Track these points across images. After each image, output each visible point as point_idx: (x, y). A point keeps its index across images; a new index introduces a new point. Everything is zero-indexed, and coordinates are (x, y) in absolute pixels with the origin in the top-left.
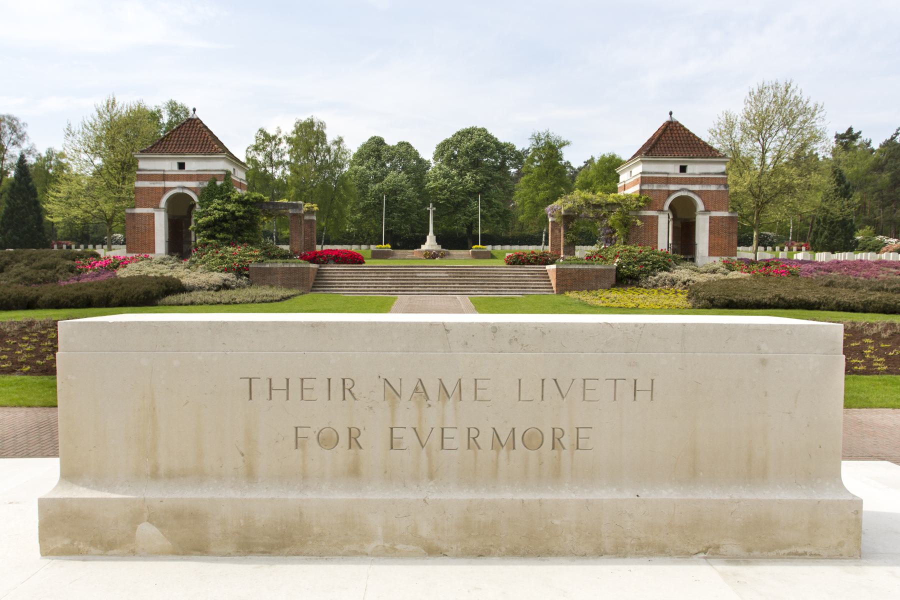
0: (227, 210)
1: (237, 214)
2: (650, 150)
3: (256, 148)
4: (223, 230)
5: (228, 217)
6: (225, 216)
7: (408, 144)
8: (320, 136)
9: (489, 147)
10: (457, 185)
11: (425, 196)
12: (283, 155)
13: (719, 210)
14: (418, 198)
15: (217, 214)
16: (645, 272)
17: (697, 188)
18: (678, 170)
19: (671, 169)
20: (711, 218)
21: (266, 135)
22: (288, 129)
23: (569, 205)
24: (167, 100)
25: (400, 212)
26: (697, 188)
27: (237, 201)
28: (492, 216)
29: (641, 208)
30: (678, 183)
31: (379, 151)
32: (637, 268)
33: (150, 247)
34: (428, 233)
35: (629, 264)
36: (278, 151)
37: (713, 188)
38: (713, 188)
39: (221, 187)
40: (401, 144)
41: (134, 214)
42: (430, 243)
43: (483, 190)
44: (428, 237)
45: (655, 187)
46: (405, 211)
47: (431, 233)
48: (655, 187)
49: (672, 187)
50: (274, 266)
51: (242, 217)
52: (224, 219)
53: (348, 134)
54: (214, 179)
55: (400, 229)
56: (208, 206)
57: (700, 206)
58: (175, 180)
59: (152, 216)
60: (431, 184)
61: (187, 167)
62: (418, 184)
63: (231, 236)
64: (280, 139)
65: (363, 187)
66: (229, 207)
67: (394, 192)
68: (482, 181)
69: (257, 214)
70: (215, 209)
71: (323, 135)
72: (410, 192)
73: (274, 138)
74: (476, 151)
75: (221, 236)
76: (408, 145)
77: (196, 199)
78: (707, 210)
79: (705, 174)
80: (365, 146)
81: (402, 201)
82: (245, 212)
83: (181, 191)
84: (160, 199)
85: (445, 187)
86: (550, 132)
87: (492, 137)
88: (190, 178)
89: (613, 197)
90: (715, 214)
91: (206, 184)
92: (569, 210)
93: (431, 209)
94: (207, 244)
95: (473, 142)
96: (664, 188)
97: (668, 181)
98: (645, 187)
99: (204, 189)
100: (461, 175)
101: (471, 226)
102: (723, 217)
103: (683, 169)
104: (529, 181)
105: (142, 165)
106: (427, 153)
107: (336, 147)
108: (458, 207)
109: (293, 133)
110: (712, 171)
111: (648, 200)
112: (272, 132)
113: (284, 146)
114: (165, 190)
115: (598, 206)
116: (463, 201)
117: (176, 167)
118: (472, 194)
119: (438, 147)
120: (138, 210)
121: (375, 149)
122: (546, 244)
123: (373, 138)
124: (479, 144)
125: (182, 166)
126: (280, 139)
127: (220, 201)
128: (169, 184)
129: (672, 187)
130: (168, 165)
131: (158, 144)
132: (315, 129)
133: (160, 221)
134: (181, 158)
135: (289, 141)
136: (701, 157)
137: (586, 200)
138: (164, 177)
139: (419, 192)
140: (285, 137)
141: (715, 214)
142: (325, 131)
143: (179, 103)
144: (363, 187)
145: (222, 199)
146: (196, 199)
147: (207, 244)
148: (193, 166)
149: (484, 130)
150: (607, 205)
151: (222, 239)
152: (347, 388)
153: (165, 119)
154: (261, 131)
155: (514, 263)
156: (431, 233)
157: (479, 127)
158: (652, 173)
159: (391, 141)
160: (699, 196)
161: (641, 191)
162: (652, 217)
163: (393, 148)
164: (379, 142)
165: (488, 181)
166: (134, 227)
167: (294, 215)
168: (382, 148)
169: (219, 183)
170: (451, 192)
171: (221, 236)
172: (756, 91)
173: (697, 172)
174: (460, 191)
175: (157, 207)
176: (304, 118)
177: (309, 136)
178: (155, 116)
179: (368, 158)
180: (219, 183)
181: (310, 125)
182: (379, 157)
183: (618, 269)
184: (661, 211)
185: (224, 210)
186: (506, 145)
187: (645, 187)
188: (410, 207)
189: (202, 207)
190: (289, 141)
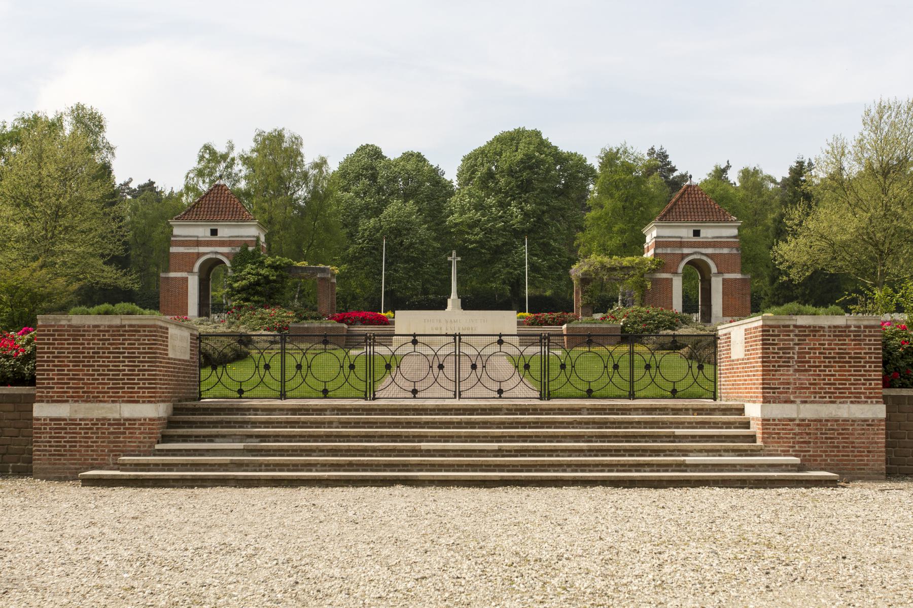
0: (261, 275)
1: (271, 278)
2: (665, 215)
3: (200, 173)
4: (257, 293)
5: (262, 281)
6: (259, 280)
7: (419, 155)
8: (293, 155)
9: (543, 162)
10: (495, 220)
11: (442, 232)
12: (238, 181)
13: (732, 272)
14: (435, 239)
15: (252, 279)
16: (647, 330)
17: (710, 251)
18: (691, 234)
19: (685, 233)
20: (724, 280)
21: (213, 153)
22: (245, 145)
23: (585, 268)
24: (72, 104)
25: (406, 262)
26: (710, 251)
27: (269, 266)
28: (550, 268)
29: (655, 271)
30: (691, 247)
31: (373, 168)
32: (641, 327)
33: (182, 309)
34: (449, 295)
35: (635, 323)
36: (229, 176)
37: (725, 251)
38: (725, 251)
39: (253, 252)
40: (408, 156)
41: (168, 278)
42: (453, 300)
43: (534, 230)
44: (449, 301)
45: (669, 251)
46: (413, 260)
47: (454, 295)
48: (669, 251)
49: (686, 251)
50: (312, 325)
51: (274, 281)
52: (257, 283)
53: (327, 146)
54: (246, 245)
55: (407, 288)
56: (241, 271)
57: (714, 269)
58: (208, 246)
59: (186, 279)
60: (455, 218)
61: (220, 233)
62: (434, 217)
63: (263, 299)
64: (233, 160)
65: (351, 223)
66: (262, 272)
67: (398, 231)
68: (534, 212)
69: (287, 278)
70: (249, 273)
71: (299, 154)
72: (422, 230)
73: (224, 157)
74: (525, 168)
75: (256, 298)
76: (420, 158)
77: (228, 264)
78: (720, 273)
79: (717, 237)
80: (350, 160)
81: (411, 244)
82: (277, 276)
83: (214, 256)
84: (193, 264)
85: (476, 223)
86: (628, 146)
87: (547, 145)
88: (222, 243)
89: (629, 261)
90: (728, 276)
91: (238, 250)
92: (585, 274)
93: (454, 259)
94: (242, 306)
95: (519, 156)
96: (678, 251)
97: (681, 244)
98: (659, 251)
99: (236, 255)
100: (502, 205)
101: (517, 285)
102: (736, 279)
103: (697, 233)
104: (599, 218)
105: (176, 231)
106: (451, 175)
107: (316, 171)
108: (497, 252)
109: (253, 151)
110: (724, 235)
111: (662, 264)
112: (221, 149)
113: (240, 169)
114: (199, 255)
115: (613, 269)
116: (504, 244)
117: (208, 233)
118: (518, 234)
119: (467, 159)
120: (172, 275)
121: (368, 164)
122: (210, 269)
123: (363, 148)
124: (529, 157)
125: (214, 232)
126: (233, 160)
127: (254, 267)
128: (202, 249)
129: (686, 251)
130: (201, 232)
131: (189, 211)
132: (285, 145)
133: (193, 283)
134: (213, 225)
135: (246, 161)
136: (713, 221)
137: (601, 263)
138: (198, 243)
139: (435, 230)
140: (242, 157)
141: (728, 276)
142: (302, 150)
143: (87, 106)
144: (351, 223)
145: (254, 263)
146: (228, 264)
147: (242, 306)
148: (226, 232)
149: (538, 134)
150: (622, 268)
151: (257, 302)
152: (440, 321)
153: (68, 128)
154: (207, 148)
155: (533, 324)
156: (454, 295)
157: (529, 128)
158: (665, 237)
159: (392, 152)
160: (712, 259)
161: (655, 255)
162: (667, 279)
163: (397, 163)
164: (375, 153)
165: (543, 212)
166: (168, 291)
167: (322, 279)
168: (380, 164)
169: (250, 249)
170: (489, 231)
171: (256, 298)
172: (874, 112)
173: (709, 236)
174: (499, 229)
175: (191, 271)
176: (269, 129)
177: (277, 153)
178: (55, 126)
179: (358, 177)
180: (250, 249)
181: (278, 137)
182: (374, 178)
183: (623, 328)
184: (675, 273)
185: (258, 274)
186: (571, 156)
187: (659, 251)
188: (423, 253)
189: (234, 271)
190: (246, 161)
